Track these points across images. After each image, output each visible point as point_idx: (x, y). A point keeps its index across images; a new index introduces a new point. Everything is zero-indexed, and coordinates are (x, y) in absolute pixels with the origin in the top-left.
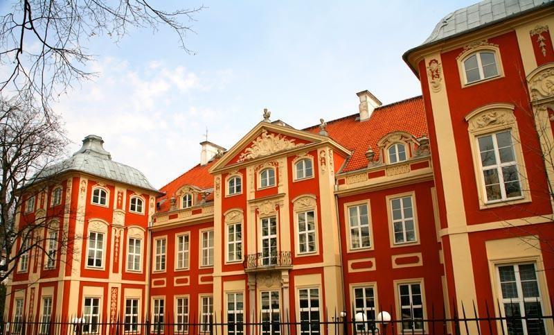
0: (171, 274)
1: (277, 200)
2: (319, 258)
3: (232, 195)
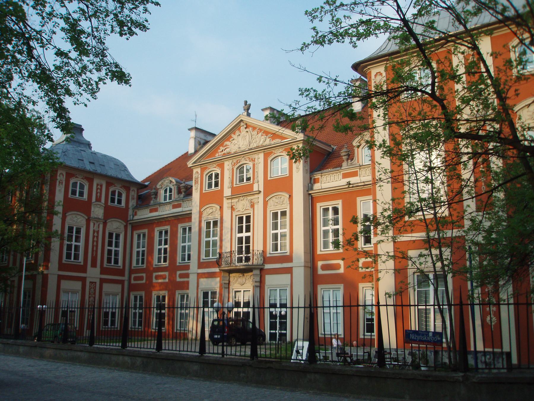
3: (210, 190)
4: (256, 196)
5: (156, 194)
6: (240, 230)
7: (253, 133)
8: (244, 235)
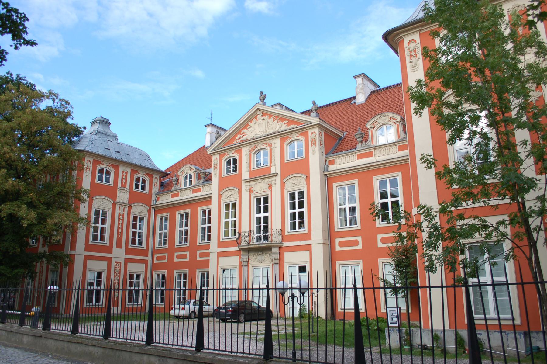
0: (172, 250)
1: (270, 180)
2: (308, 236)
4: (274, 178)
5: (177, 181)
6: (259, 211)
7: (269, 120)
8: (262, 215)
